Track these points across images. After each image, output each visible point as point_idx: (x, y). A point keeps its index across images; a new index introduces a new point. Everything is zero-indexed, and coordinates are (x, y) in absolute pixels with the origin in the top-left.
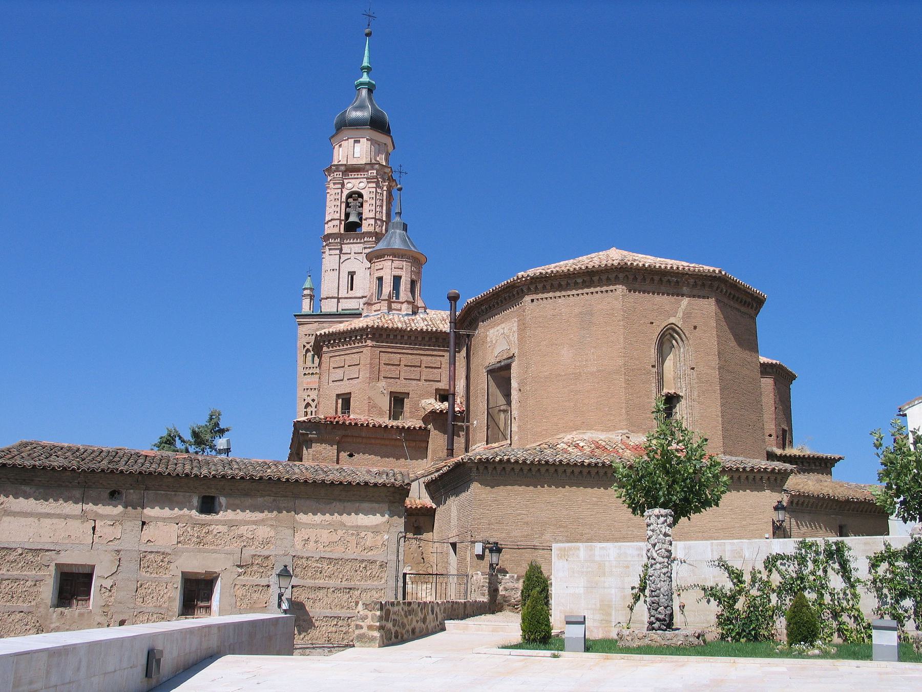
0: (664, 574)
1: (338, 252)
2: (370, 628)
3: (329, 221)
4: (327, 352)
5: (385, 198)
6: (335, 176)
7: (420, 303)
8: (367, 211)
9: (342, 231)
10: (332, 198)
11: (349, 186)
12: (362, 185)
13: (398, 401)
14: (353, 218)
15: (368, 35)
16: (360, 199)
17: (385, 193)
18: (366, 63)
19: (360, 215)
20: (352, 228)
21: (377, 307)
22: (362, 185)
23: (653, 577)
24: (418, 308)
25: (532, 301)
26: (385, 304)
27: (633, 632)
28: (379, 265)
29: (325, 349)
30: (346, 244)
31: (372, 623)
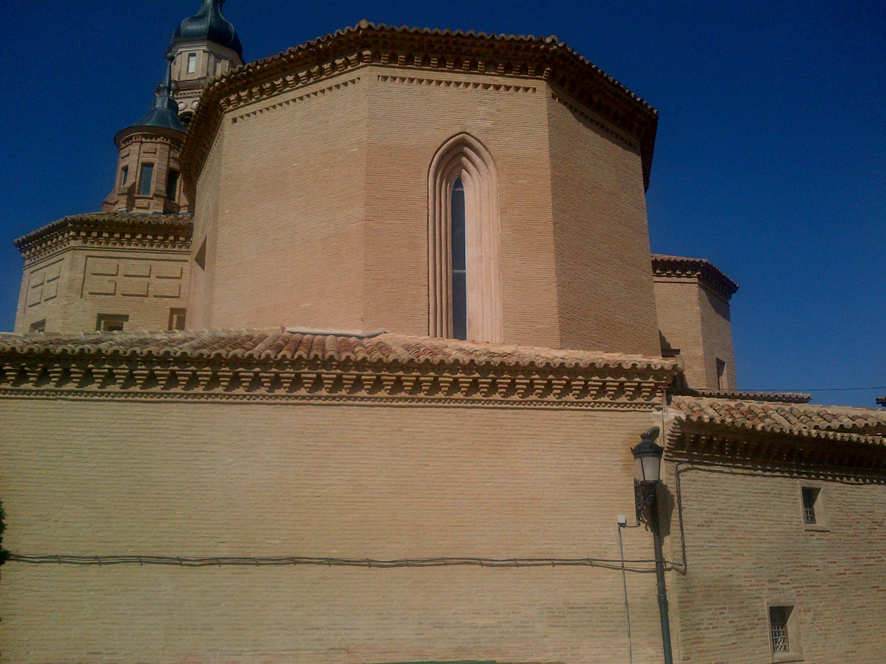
4: (29, 266)
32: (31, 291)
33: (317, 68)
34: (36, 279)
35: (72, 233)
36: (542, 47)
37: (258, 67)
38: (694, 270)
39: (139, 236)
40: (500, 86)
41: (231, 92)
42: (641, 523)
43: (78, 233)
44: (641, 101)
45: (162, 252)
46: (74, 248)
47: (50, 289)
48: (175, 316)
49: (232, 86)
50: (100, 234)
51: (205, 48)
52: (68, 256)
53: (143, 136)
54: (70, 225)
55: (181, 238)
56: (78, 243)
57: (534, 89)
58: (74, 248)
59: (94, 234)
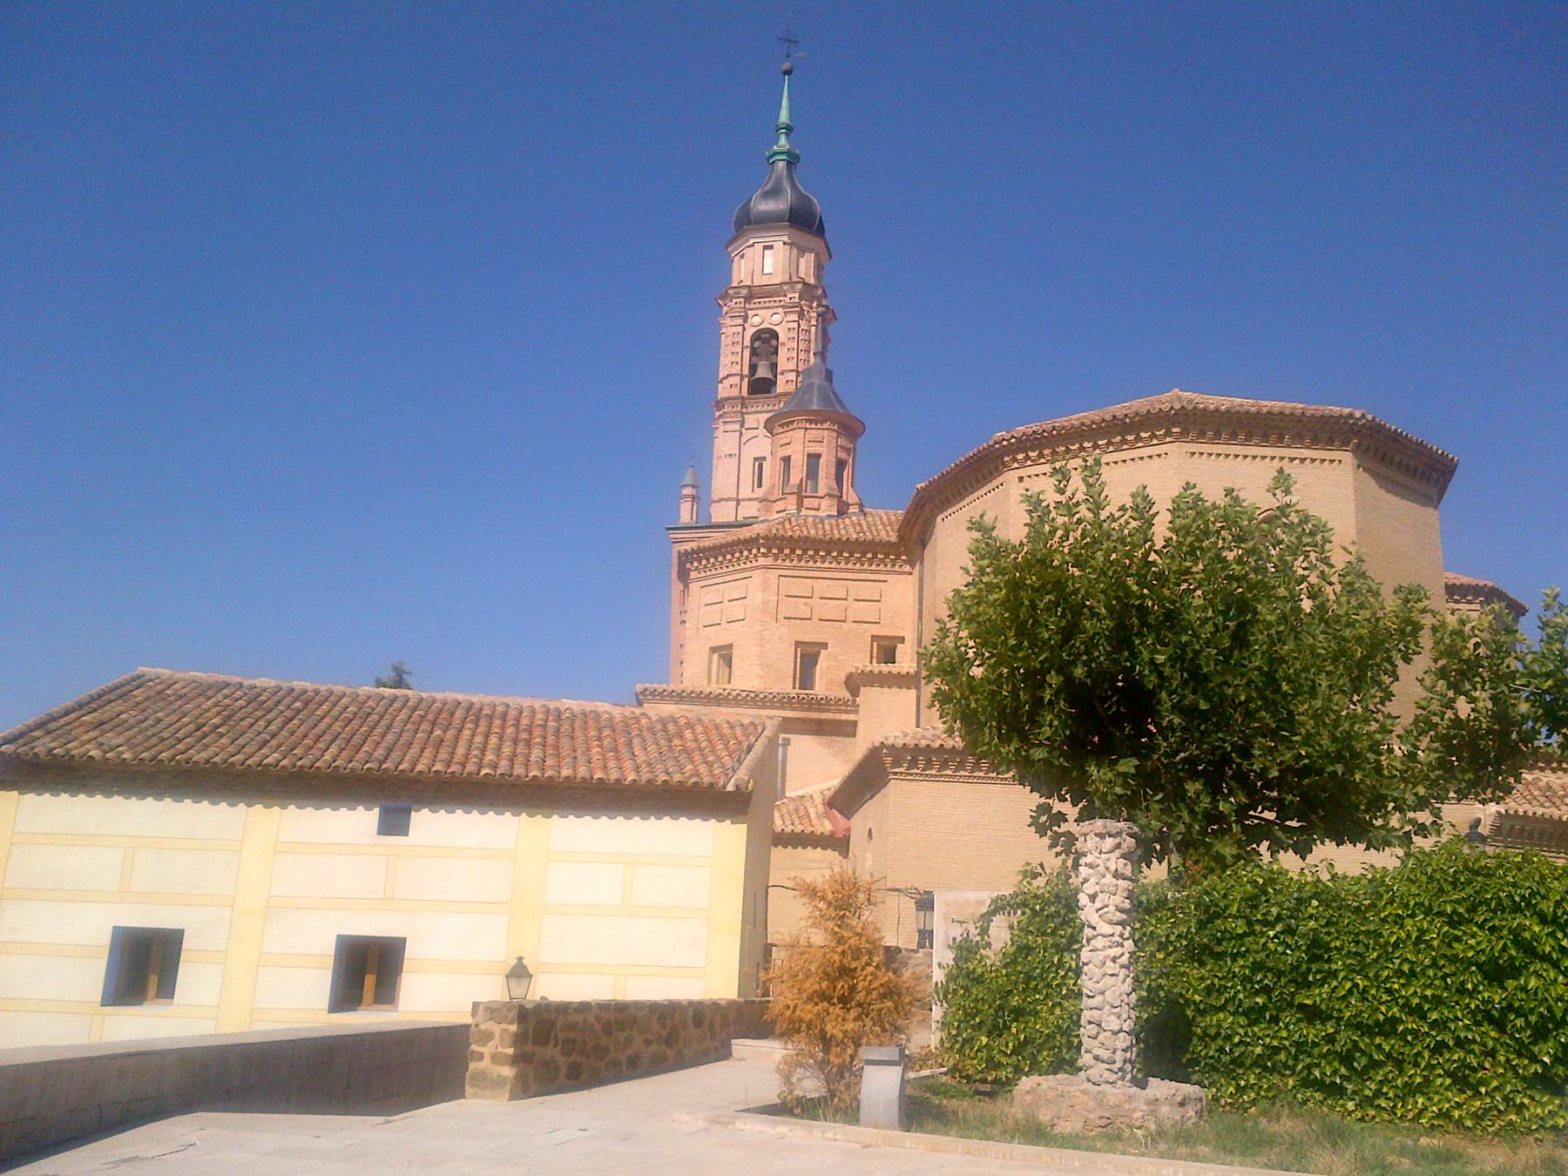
0: (1114, 960)
1: (737, 427)
2: (496, 1059)
3: (725, 378)
4: (698, 579)
5: (813, 337)
6: (734, 306)
7: (850, 496)
8: (785, 359)
9: (745, 392)
10: (729, 341)
11: (757, 320)
12: (776, 318)
13: (808, 657)
14: (762, 372)
15: (788, 72)
16: (774, 342)
17: (813, 329)
18: (784, 117)
19: (774, 366)
20: (761, 387)
21: (779, 506)
22: (776, 318)
23: (1091, 965)
24: (849, 505)
25: (1021, 479)
26: (793, 499)
27: (1039, 1085)
28: (784, 438)
29: (693, 575)
30: (751, 413)
31: (500, 1049)
32: (703, 609)
33: (1119, 438)
34: (711, 595)
35: (762, 550)
36: (1352, 421)
37: (1054, 432)
38: (1477, 596)
39: (835, 554)
40: (1306, 459)
41: (1019, 451)
42: (1104, 832)
43: (769, 550)
44: (1443, 453)
45: (859, 571)
46: (766, 567)
47: (737, 610)
48: (875, 644)
49: (1021, 446)
50: (793, 551)
51: (785, 239)
52: (757, 574)
53: (807, 420)
54: (761, 541)
55: (879, 556)
56: (769, 561)
57: (1340, 461)
58: (766, 567)
59: (787, 551)
